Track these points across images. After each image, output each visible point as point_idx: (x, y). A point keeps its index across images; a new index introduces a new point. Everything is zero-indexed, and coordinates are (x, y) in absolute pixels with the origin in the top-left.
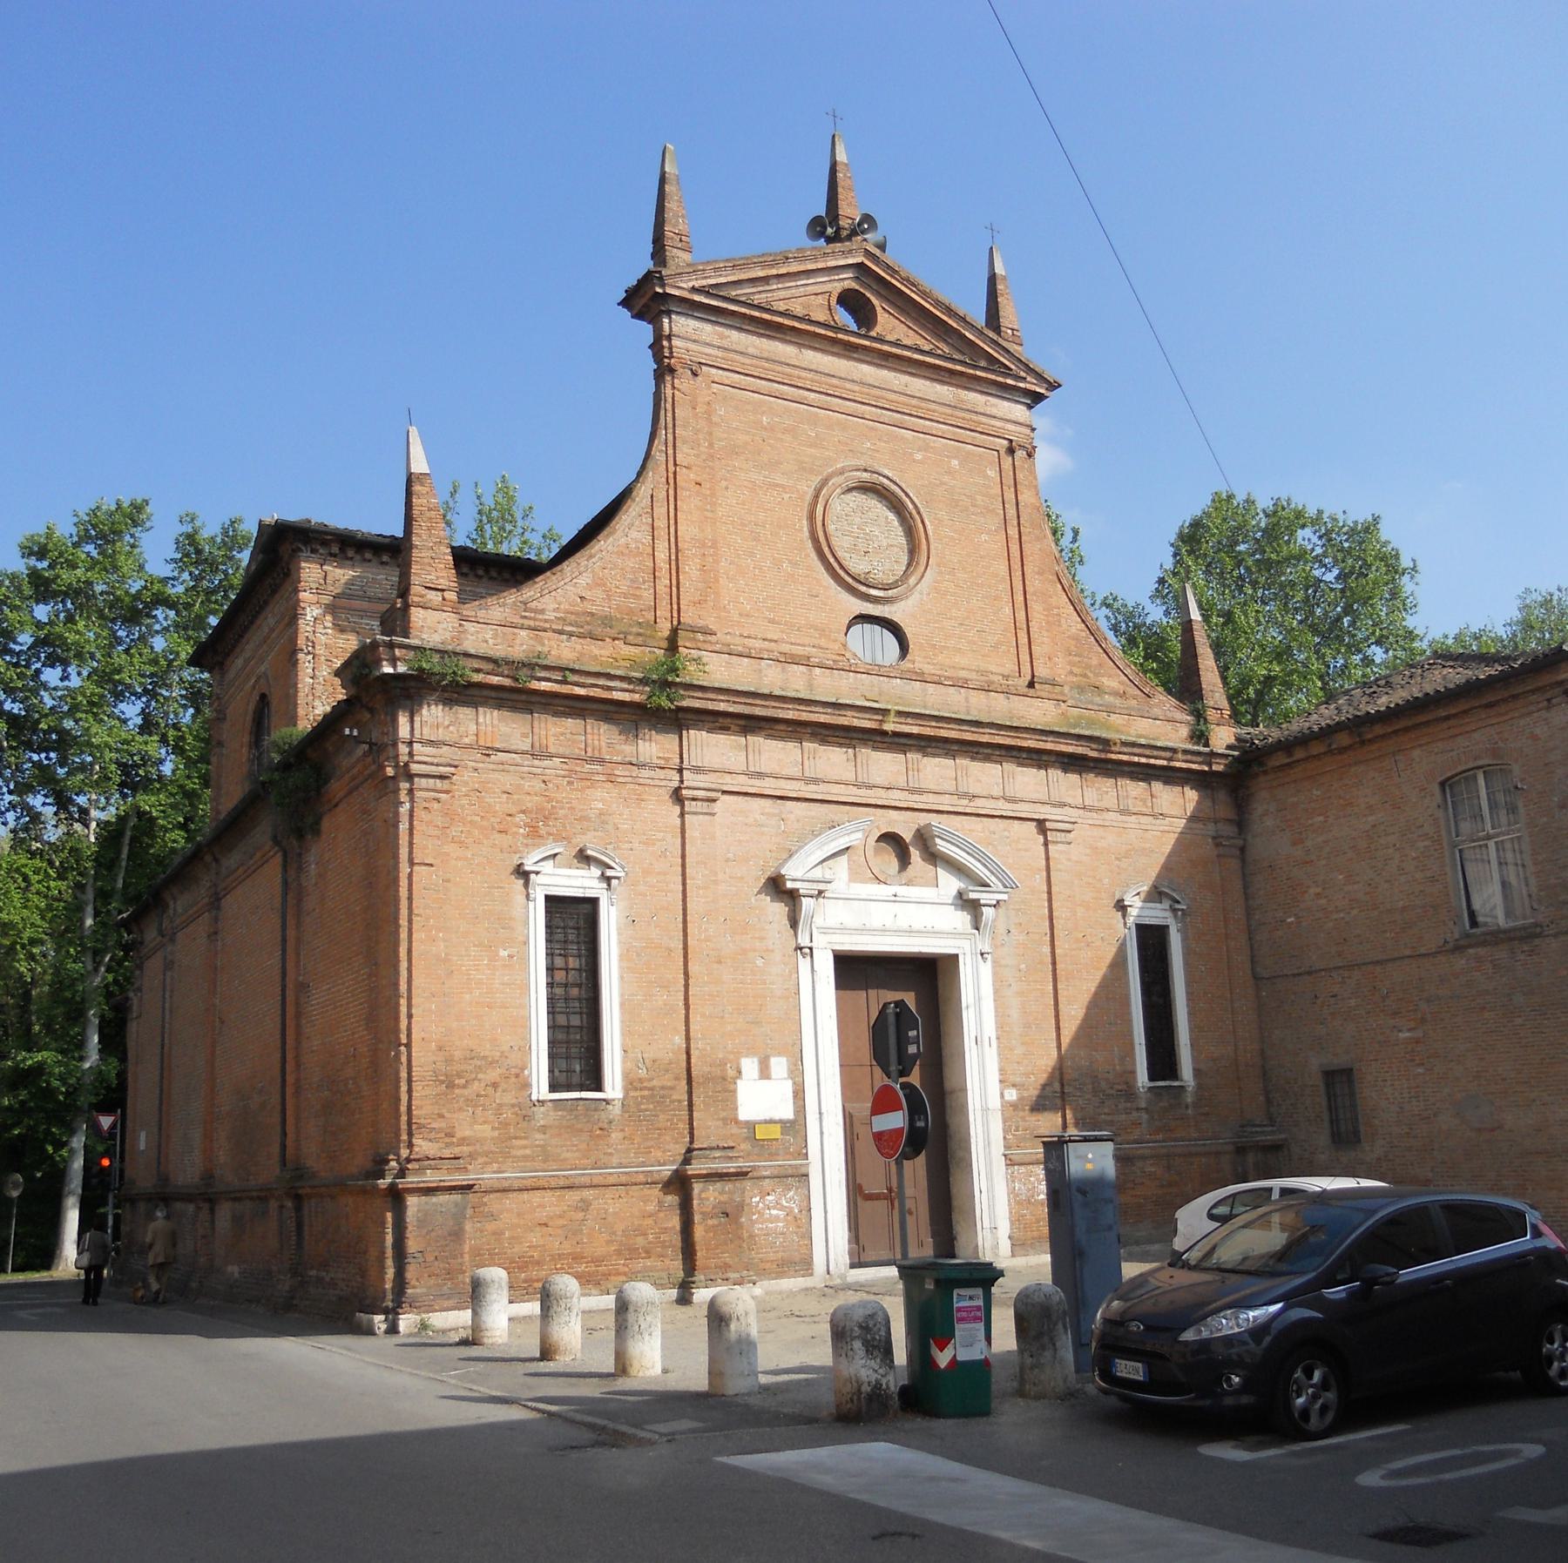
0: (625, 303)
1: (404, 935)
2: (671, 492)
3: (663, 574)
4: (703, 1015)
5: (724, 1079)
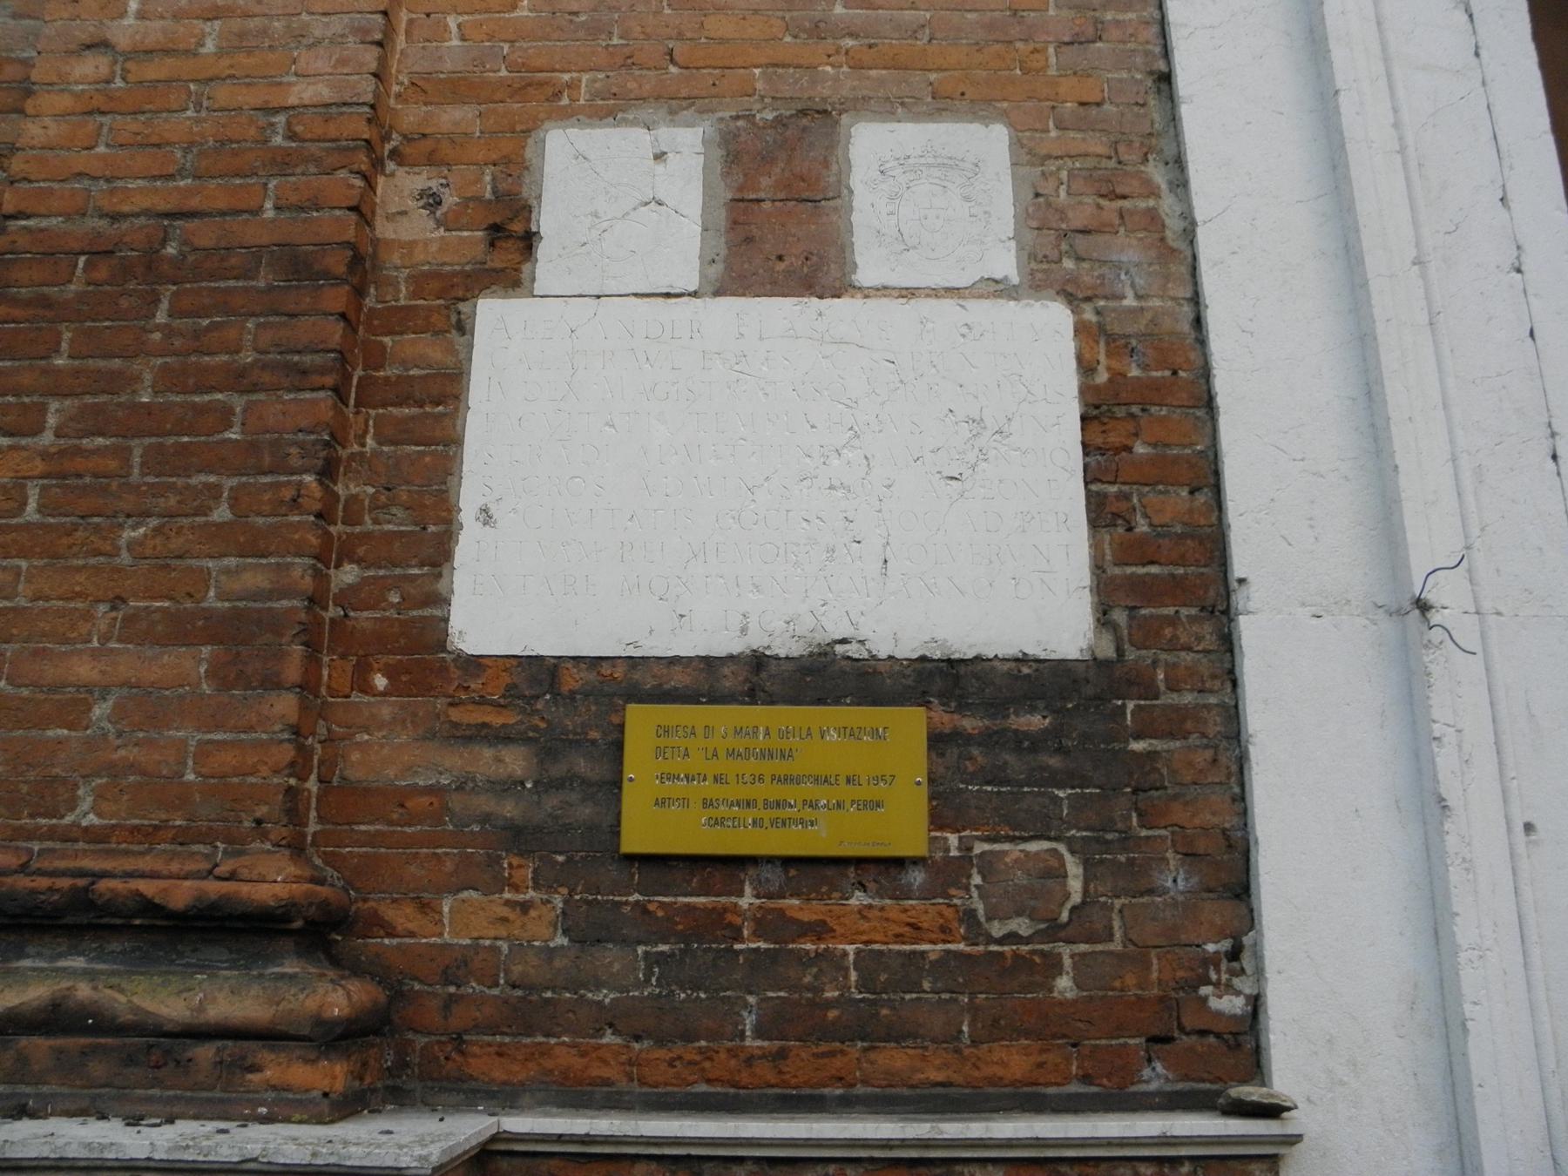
5: (362, 264)
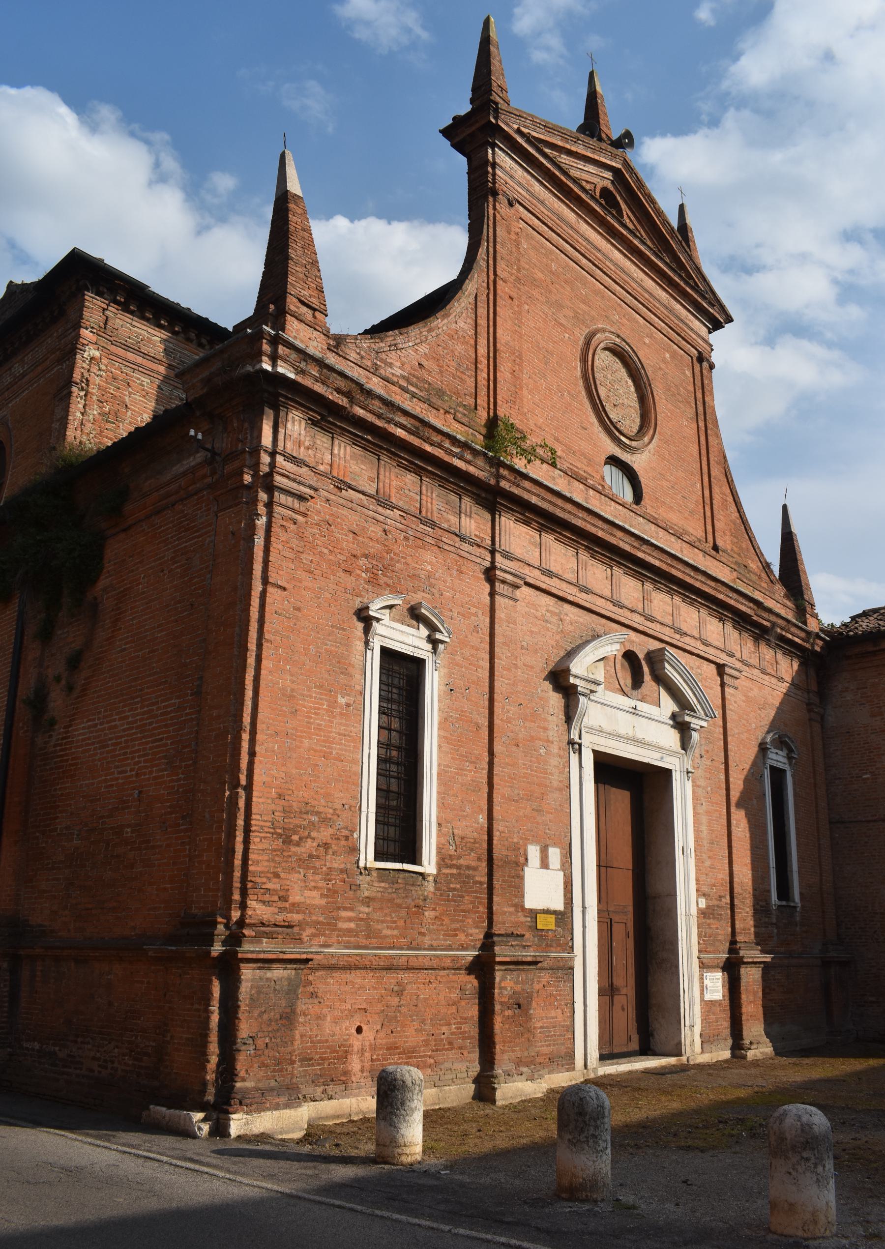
0: (447, 132)
1: (251, 660)
2: (491, 297)
3: (483, 366)
4: (503, 796)
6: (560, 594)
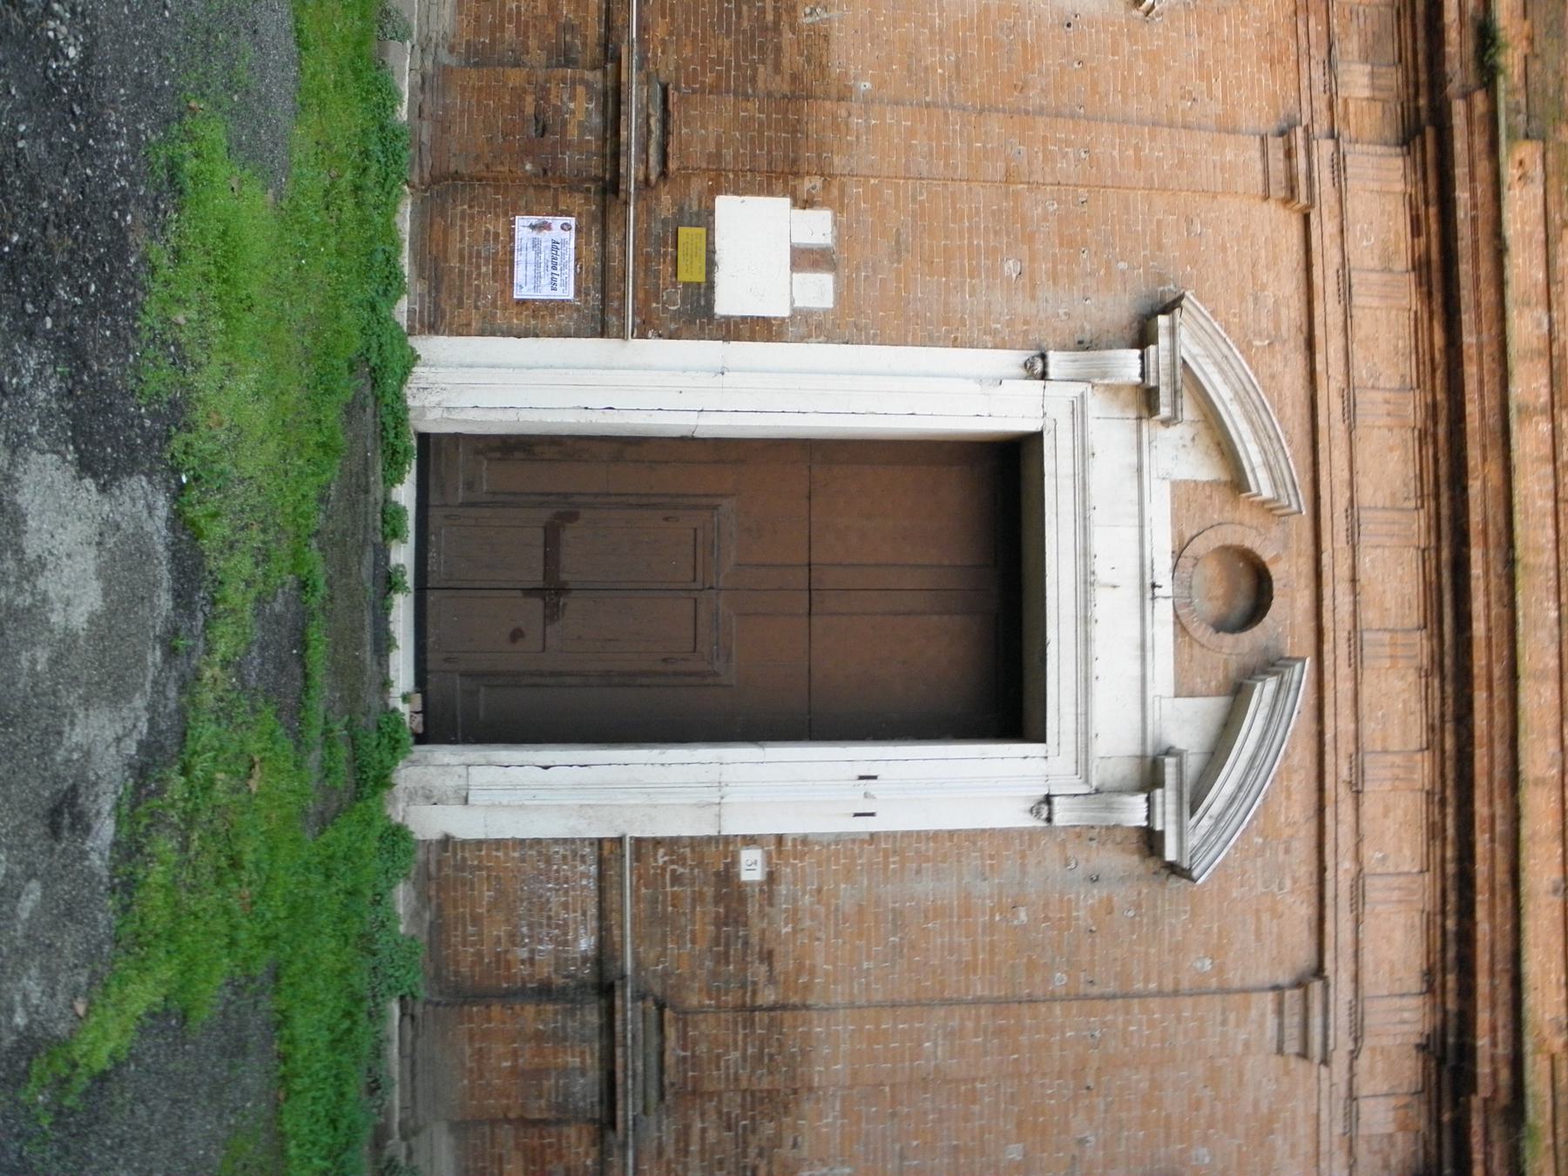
4: (911, 132)
6: (1319, 332)
